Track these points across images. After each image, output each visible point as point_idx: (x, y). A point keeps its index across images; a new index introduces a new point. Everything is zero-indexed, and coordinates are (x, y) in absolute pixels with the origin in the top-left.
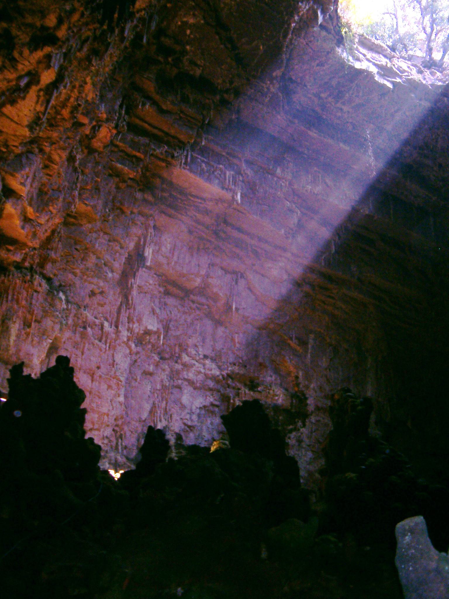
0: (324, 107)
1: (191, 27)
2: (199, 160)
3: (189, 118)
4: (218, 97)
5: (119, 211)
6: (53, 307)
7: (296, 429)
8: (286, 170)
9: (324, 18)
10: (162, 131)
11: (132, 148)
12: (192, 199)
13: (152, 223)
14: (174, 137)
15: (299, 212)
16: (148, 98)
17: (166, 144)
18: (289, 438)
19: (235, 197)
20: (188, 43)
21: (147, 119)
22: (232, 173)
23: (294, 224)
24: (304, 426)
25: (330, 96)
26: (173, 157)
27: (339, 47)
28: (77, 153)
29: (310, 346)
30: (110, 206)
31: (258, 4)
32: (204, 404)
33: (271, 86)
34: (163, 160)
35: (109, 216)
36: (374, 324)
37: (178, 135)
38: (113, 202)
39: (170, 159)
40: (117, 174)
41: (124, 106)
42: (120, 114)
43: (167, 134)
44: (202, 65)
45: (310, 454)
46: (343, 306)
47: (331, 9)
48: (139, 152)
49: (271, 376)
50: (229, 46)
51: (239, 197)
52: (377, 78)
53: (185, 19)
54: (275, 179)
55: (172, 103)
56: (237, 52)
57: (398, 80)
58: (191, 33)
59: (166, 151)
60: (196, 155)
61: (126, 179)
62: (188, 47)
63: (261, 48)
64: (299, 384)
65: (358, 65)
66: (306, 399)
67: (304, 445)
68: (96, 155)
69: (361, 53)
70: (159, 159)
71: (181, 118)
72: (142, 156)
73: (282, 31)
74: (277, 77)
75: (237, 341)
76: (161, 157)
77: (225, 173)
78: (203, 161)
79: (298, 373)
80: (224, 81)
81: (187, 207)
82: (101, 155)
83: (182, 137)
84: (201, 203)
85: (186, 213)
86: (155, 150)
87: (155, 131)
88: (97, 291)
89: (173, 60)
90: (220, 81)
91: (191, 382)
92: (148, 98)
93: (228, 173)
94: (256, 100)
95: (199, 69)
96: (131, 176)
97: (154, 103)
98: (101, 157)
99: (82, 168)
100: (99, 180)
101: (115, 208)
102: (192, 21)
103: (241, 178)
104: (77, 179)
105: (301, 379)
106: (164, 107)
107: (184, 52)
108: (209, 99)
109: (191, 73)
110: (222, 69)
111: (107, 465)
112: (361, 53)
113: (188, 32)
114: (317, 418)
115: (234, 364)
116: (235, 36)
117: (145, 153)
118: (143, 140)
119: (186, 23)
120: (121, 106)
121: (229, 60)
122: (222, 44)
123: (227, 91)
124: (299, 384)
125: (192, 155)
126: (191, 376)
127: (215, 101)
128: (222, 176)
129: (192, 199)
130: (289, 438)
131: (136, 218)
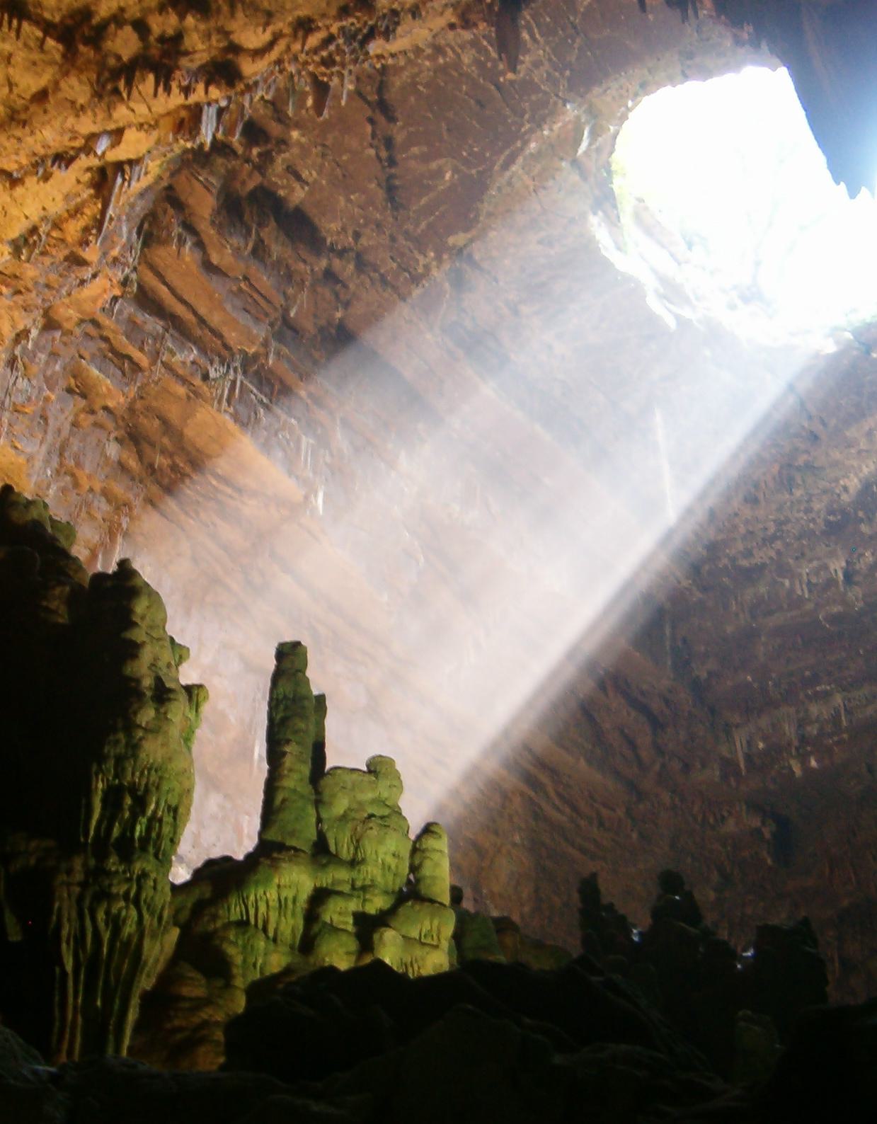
3: (256, 296)
4: (324, 263)
5: (68, 478)
9: (590, 144)
10: (195, 313)
11: (127, 337)
12: (214, 482)
14: (216, 333)
15: (422, 559)
16: (190, 228)
17: (195, 343)
19: (312, 498)
20: (297, 125)
21: (171, 277)
22: (311, 441)
26: (206, 377)
27: (595, 214)
30: (55, 464)
31: (482, 81)
33: (434, 263)
34: (184, 381)
35: (48, 487)
36: (517, 839)
37: (225, 331)
38: (61, 455)
39: (197, 381)
40: (80, 389)
43: (202, 321)
44: (310, 180)
47: (609, 129)
48: (141, 349)
50: (384, 154)
55: (237, 251)
56: (393, 171)
59: (193, 363)
61: (97, 407)
62: (295, 134)
63: (448, 176)
68: (58, 334)
70: (177, 376)
71: (240, 290)
72: (144, 361)
73: (507, 152)
75: (246, 831)
76: (181, 372)
77: (298, 442)
78: (261, 402)
80: (344, 229)
81: (201, 499)
82: (65, 339)
83: (232, 337)
84: (231, 497)
85: (197, 513)
86: (173, 353)
87: (180, 310)
90: (334, 226)
94: (393, 287)
95: (303, 188)
96: (111, 404)
97: (200, 244)
98: (65, 344)
99: (26, 360)
100: (53, 397)
101: (63, 470)
103: (328, 459)
106: (215, 259)
107: (283, 143)
108: (305, 261)
109: (282, 193)
110: (349, 200)
116: (399, 138)
117: (155, 356)
118: (153, 324)
121: (373, 186)
122: (371, 146)
123: (341, 253)
127: (316, 269)
129: (214, 482)
131: (96, 503)
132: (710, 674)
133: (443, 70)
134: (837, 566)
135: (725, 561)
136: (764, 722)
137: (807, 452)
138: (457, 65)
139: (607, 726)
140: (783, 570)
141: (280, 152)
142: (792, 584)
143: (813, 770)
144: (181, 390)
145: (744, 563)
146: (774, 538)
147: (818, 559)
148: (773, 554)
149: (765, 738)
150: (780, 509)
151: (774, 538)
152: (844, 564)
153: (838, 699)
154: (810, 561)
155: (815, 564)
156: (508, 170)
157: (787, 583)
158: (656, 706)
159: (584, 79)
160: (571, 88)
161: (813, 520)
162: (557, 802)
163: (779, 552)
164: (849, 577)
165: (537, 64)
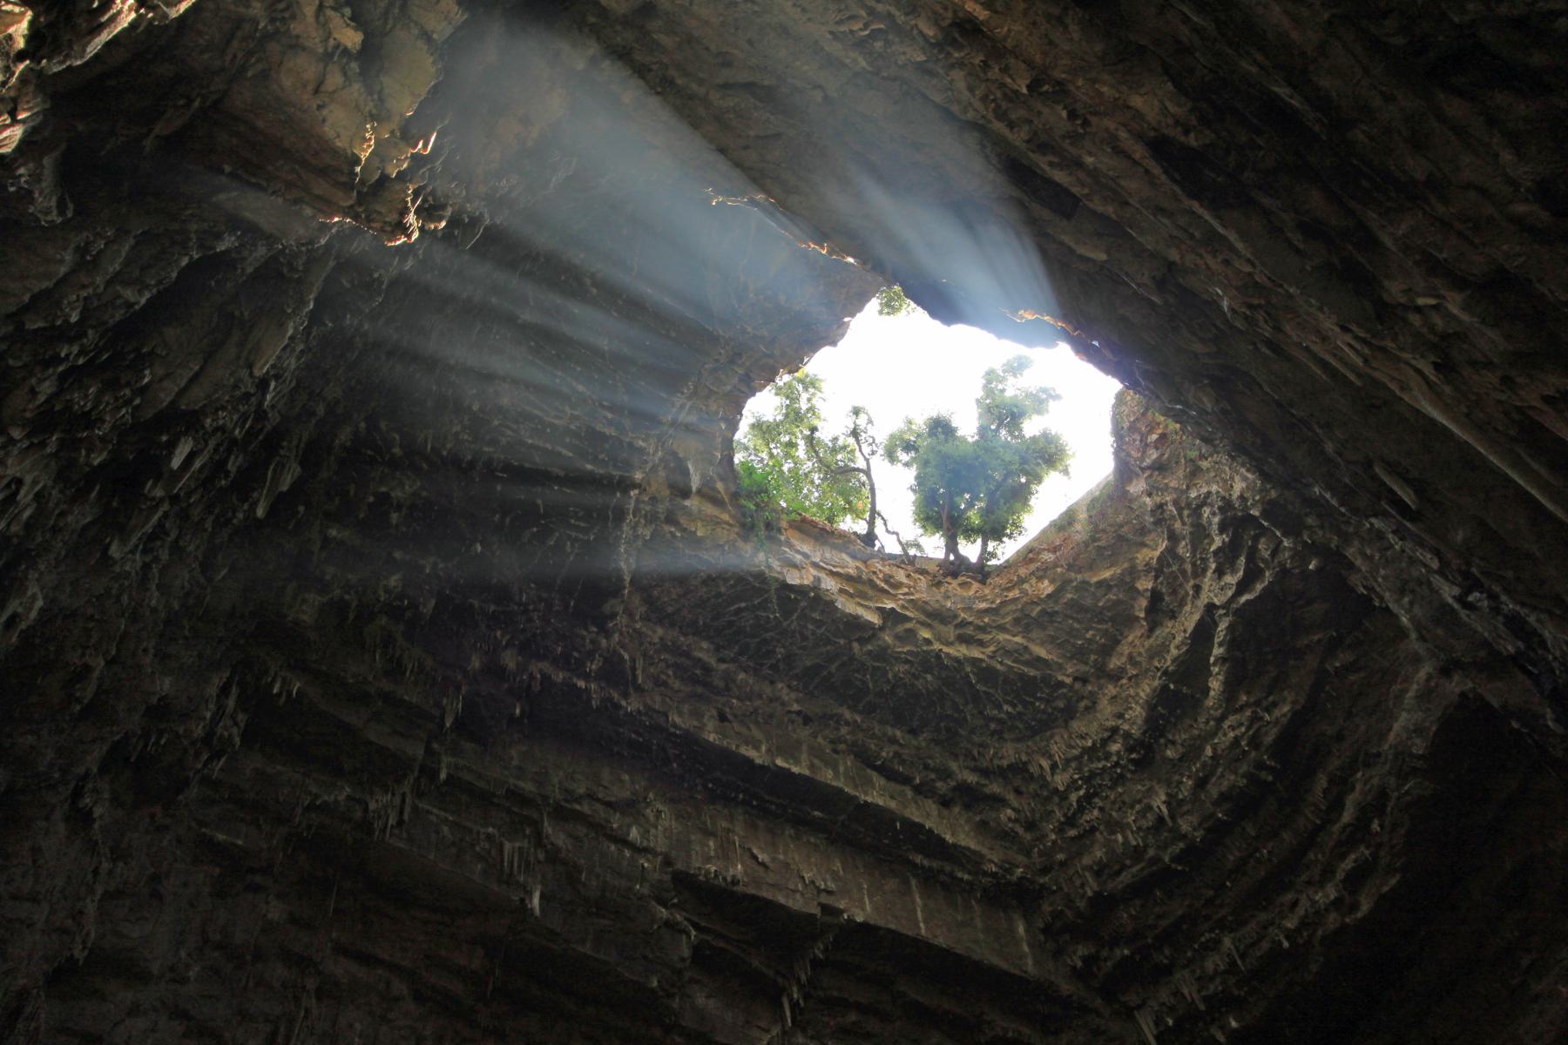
2: (434, 819)
8: (653, 831)
13: (311, 984)
23: (683, 960)
25: (741, 653)
28: (95, 803)
35: (188, 966)
41: (234, 690)
42: (221, 708)
51: (536, 901)
53: (383, 489)
54: (627, 853)
57: (889, 605)
60: (427, 807)
69: (798, 552)
77: (501, 845)
93: (507, 846)
104: (96, 872)
111: (1289, 699)
112: (798, 552)
113: (394, 517)
119: (386, 496)
120: (225, 690)
125: (415, 809)
128: (493, 853)
132: (1085, 959)
134: (1159, 801)
136: (1164, 995)
142: (1125, 837)
143: (1235, 1031)
147: (1140, 801)
149: (1172, 1009)
152: (1163, 798)
153: (1227, 942)
154: (1132, 807)
155: (1138, 807)
156: (832, 602)
157: (1120, 838)
161: (1117, 764)
163: (1101, 809)
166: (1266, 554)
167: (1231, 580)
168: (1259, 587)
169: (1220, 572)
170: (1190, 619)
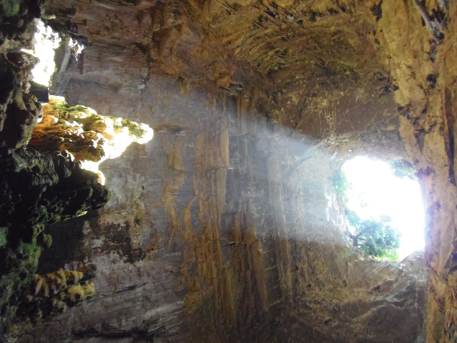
0: (296, 198)
1: (291, 101)
6: (139, 224)
7: (121, 256)
9: (335, 158)
18: (114, 253)
20: (284, 107)
24: (125, 262)
25: (304, 196)
29: (173, 254)
32: (116, 193)
34: (228, 123)
45: (108, 272)
46: (205, 269)
49: (147, 232)
52: (327, 209)
53: (293, 96)
57: (334, 222)
58: (289, 104)
59: (232, 123)
62: (282, 109)
64: (150, 252)
65: (326, 195)
66: (142, 259)
67: (113, 265)
74: (295, 159)
79: (156, 249)
85: (210, 149)
88: (153, 110)
89: (273, 104)
91: (126, 181)
92: (250, 99)
102: (294, 99)
105: (152, 252)
113: (289, 102)
114: (133, 271)
115: (145, 207)
124: (150, 252)
126: (130, 179)
130: (114, 253)
133: (315, 113)
134: (327, 318)
135: (304, 299)
137: (342, 288)
138: (317, 113)
139: (246, 302)
140: (315, 311)
141: (278, 110)
144: (226, 124)
145: (308, 304)
146: (319, 303)
148: (315, 307)
150: (325, 296)
151: (319, 303)
158: (261, 313)
159: (340, 131)
160: (336, 131)
161: (330, 304)
162: (220, 301)
163: (317, 308)
164: (326, 322)
165: (332, 121)
166: (409, 303)
167: (396, 300)
168: (399, 308)
169: (396, 297)
170: (380, 298)
